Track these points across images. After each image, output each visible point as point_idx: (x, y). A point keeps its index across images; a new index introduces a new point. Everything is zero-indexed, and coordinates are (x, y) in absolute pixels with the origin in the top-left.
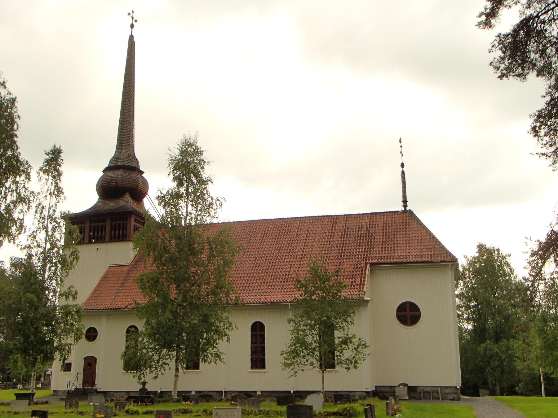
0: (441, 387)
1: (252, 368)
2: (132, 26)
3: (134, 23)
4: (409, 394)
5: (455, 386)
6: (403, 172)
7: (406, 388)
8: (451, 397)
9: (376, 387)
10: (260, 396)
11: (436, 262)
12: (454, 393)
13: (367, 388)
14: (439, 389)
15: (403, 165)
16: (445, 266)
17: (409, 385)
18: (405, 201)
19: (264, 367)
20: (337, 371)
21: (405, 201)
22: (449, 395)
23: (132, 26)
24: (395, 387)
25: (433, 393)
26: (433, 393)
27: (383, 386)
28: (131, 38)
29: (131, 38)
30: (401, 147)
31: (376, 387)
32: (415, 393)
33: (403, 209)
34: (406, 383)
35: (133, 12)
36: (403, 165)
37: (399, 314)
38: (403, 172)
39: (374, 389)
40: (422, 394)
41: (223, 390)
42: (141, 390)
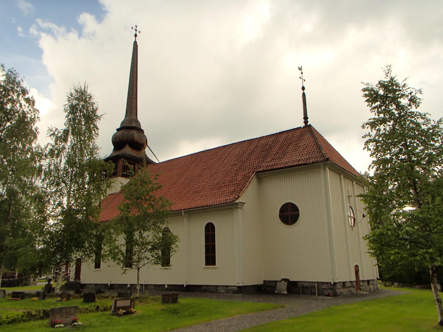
0: (318, 283)
1: (206, 265)
2: (136, 36)
3: (138, 33)
4: (288, 289)
5: (330, 281)
6: (304, 95)
7: (286, 283)
8: (326, 292)
9: (264, 281)
10: (167, 288)
11: (309, 164)
12: (330, 289)
13: (238, 283)
14: (316, 284)
15: (303, 88)
16: (319, 167)
17: (291, 280)
18: (306, 118)
19: (214, 264)
20: (217, 268)
21: (306, 118)
22: (326, 291)
23: (136, 36)
24: (276, 282)
25: (311, 288)
26: (311, 288)
27: (269, 281)
28: (135, 43)
29: (135, 43)
30: (302, 73)
31: (264, 281)
32: (295, 289)
33: (304, 125)
34: (288, 278)
35: (136, 26)
36: (303, 88)
37: (296, 213)
38: (304, 95)
39: (262, 283)
40: (301, 290)
41: (144, 284)
42: (46, 286)
